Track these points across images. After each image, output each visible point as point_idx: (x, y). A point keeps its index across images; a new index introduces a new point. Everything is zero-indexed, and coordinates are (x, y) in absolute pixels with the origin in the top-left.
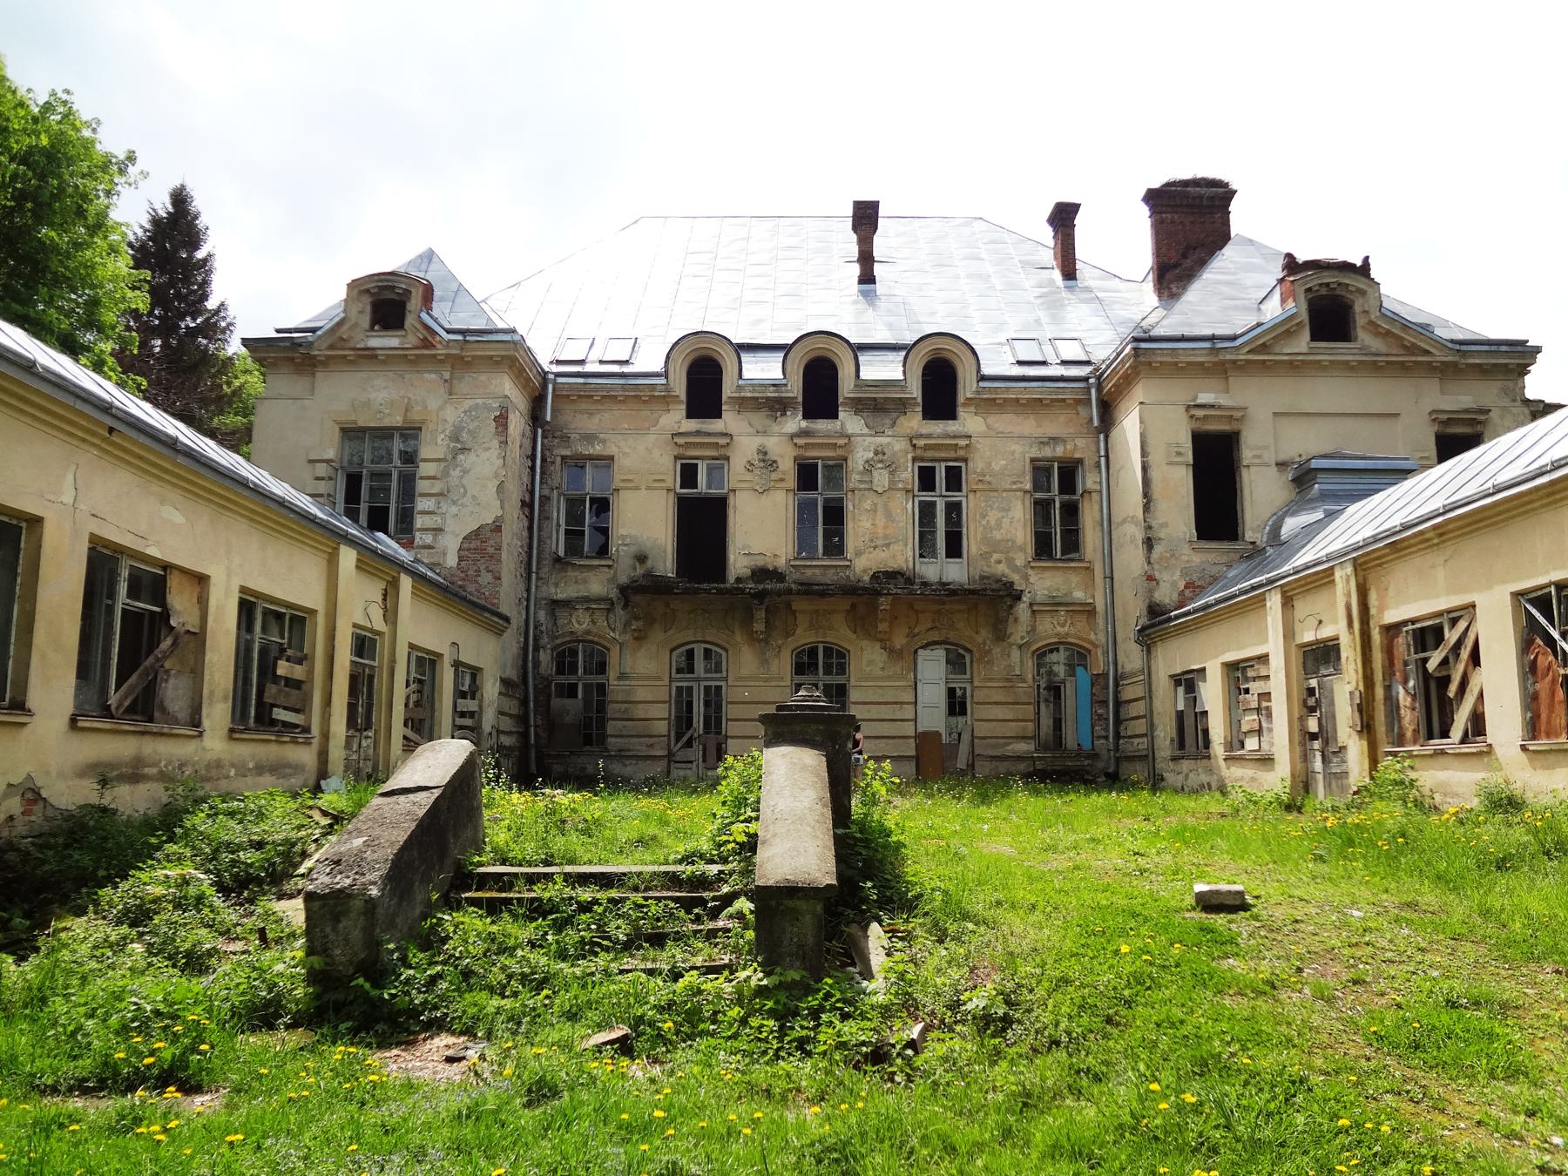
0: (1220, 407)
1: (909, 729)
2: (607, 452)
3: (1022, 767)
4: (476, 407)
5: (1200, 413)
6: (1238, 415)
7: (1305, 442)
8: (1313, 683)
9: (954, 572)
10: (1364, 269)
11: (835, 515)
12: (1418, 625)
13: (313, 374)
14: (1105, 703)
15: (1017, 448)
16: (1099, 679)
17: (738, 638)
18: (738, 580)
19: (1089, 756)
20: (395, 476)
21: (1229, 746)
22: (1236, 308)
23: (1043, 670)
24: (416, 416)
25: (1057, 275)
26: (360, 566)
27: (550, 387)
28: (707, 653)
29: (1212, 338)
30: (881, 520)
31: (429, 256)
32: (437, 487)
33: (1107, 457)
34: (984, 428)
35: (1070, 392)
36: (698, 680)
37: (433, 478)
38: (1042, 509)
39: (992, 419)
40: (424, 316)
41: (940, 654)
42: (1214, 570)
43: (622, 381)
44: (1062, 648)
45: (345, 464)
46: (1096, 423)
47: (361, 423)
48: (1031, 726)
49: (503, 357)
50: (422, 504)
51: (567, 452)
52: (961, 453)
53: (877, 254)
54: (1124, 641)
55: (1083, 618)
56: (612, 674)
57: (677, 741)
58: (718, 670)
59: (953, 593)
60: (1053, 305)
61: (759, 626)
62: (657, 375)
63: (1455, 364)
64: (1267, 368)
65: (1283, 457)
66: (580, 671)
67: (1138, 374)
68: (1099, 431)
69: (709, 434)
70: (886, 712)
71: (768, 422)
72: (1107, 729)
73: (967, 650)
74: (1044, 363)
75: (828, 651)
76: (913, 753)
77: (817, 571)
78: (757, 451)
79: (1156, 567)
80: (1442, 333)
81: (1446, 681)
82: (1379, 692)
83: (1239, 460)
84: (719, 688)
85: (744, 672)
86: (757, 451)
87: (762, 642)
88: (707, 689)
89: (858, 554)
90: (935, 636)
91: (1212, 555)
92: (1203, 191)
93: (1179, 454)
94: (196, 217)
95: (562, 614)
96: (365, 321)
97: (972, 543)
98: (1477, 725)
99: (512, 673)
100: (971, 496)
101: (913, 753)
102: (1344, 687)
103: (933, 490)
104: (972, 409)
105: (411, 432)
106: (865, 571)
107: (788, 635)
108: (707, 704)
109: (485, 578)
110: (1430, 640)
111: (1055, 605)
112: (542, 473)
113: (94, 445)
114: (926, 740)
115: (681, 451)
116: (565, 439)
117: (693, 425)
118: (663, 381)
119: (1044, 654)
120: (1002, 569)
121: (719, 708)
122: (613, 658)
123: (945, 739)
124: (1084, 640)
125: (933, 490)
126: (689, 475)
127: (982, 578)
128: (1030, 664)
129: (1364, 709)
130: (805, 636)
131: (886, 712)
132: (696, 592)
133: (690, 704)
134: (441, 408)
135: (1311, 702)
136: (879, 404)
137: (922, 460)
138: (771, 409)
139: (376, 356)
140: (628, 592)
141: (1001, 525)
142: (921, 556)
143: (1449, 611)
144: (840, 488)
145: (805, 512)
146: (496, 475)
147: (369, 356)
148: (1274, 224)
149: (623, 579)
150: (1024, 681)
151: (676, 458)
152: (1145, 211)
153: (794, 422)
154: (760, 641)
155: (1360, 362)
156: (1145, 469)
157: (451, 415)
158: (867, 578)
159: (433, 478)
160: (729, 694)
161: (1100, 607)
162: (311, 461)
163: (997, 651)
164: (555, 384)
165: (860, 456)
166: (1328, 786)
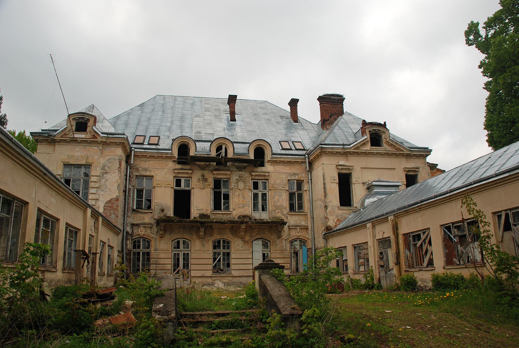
0: (346, 166)
1: (250, 267)
5: (340, 167)
7: (370, 177)
9: (264, 216)
10: (384, 125)
15: (284, 176)
17: (195, 237)
20: (82, 181)
23: (292, 247)
24: (90, 161)
28: (184, 242)
32: (97, 185)
33: (311, 180)
35: (300, 159)
36: (181, 251)
37: (96, 182)
38: (291, 195)
40: (94, 128)
41: (260, 242)
42: (345, 216)
43: (157, 151)
47: (71, 163)
49: (120, 143)
50: (92, 191)
51: (138, 174)
52: (266, 178)
53: (236, 111)
54: (318, 238)
55: (304, 230)
56: (152, 249)
57: (174, 271)
58: (188, 247)
59: (264, 223)
61: (202, 233)
63: (410, 154)
65: (364, 181)
66: (141, 247)
73: (268, 241)
74: (291, 149)
75: (224, 241)
77: (221, 215)
80: (406, 145)
83: (351, 182)
84: (188, 254)
85: (196, 248)
89: (234, 210)
91: (345, 211)
93: (334, 180)
95: (134, 228)
97: (270, 206)
98: (431, 263)
99: (120, 249)
103: (258, 189)
105: (88, 166)
106: (236, 215)
107: (211, 236)
108: (184, 259)
109: (113, 216)
110: (416, 238)
111: (295, 227)
112: (129, 181)
113: (39, 179)
115: (176, 175)
116: (137, 169)
118: (170, 152)
119: (292, 242)
120: (279, 215)
121: (188, 260)
122: (152, 243)
125: (258, 189)
126: (178, 183)
127: (273, 218)
128: (288, 245)
130: (217, 237)
132: (182, 222)
133: (178, 259)
134: (99, 158)
135: (382, 256)
137: (254, 179)
140: (158, 222)
141: (279, 202)
143: (422, 230)
144: (228, 188)
146: (117, 182)
147: (75, 141)
149: (156, 217)
150: (287, 251)
151: (174, 177)
152: (318, 103)
154: (202, 238)
157: (102, 161)
158: (237, 218)
159: (96, 182)
161: (310, 227)
163: (278, 241)
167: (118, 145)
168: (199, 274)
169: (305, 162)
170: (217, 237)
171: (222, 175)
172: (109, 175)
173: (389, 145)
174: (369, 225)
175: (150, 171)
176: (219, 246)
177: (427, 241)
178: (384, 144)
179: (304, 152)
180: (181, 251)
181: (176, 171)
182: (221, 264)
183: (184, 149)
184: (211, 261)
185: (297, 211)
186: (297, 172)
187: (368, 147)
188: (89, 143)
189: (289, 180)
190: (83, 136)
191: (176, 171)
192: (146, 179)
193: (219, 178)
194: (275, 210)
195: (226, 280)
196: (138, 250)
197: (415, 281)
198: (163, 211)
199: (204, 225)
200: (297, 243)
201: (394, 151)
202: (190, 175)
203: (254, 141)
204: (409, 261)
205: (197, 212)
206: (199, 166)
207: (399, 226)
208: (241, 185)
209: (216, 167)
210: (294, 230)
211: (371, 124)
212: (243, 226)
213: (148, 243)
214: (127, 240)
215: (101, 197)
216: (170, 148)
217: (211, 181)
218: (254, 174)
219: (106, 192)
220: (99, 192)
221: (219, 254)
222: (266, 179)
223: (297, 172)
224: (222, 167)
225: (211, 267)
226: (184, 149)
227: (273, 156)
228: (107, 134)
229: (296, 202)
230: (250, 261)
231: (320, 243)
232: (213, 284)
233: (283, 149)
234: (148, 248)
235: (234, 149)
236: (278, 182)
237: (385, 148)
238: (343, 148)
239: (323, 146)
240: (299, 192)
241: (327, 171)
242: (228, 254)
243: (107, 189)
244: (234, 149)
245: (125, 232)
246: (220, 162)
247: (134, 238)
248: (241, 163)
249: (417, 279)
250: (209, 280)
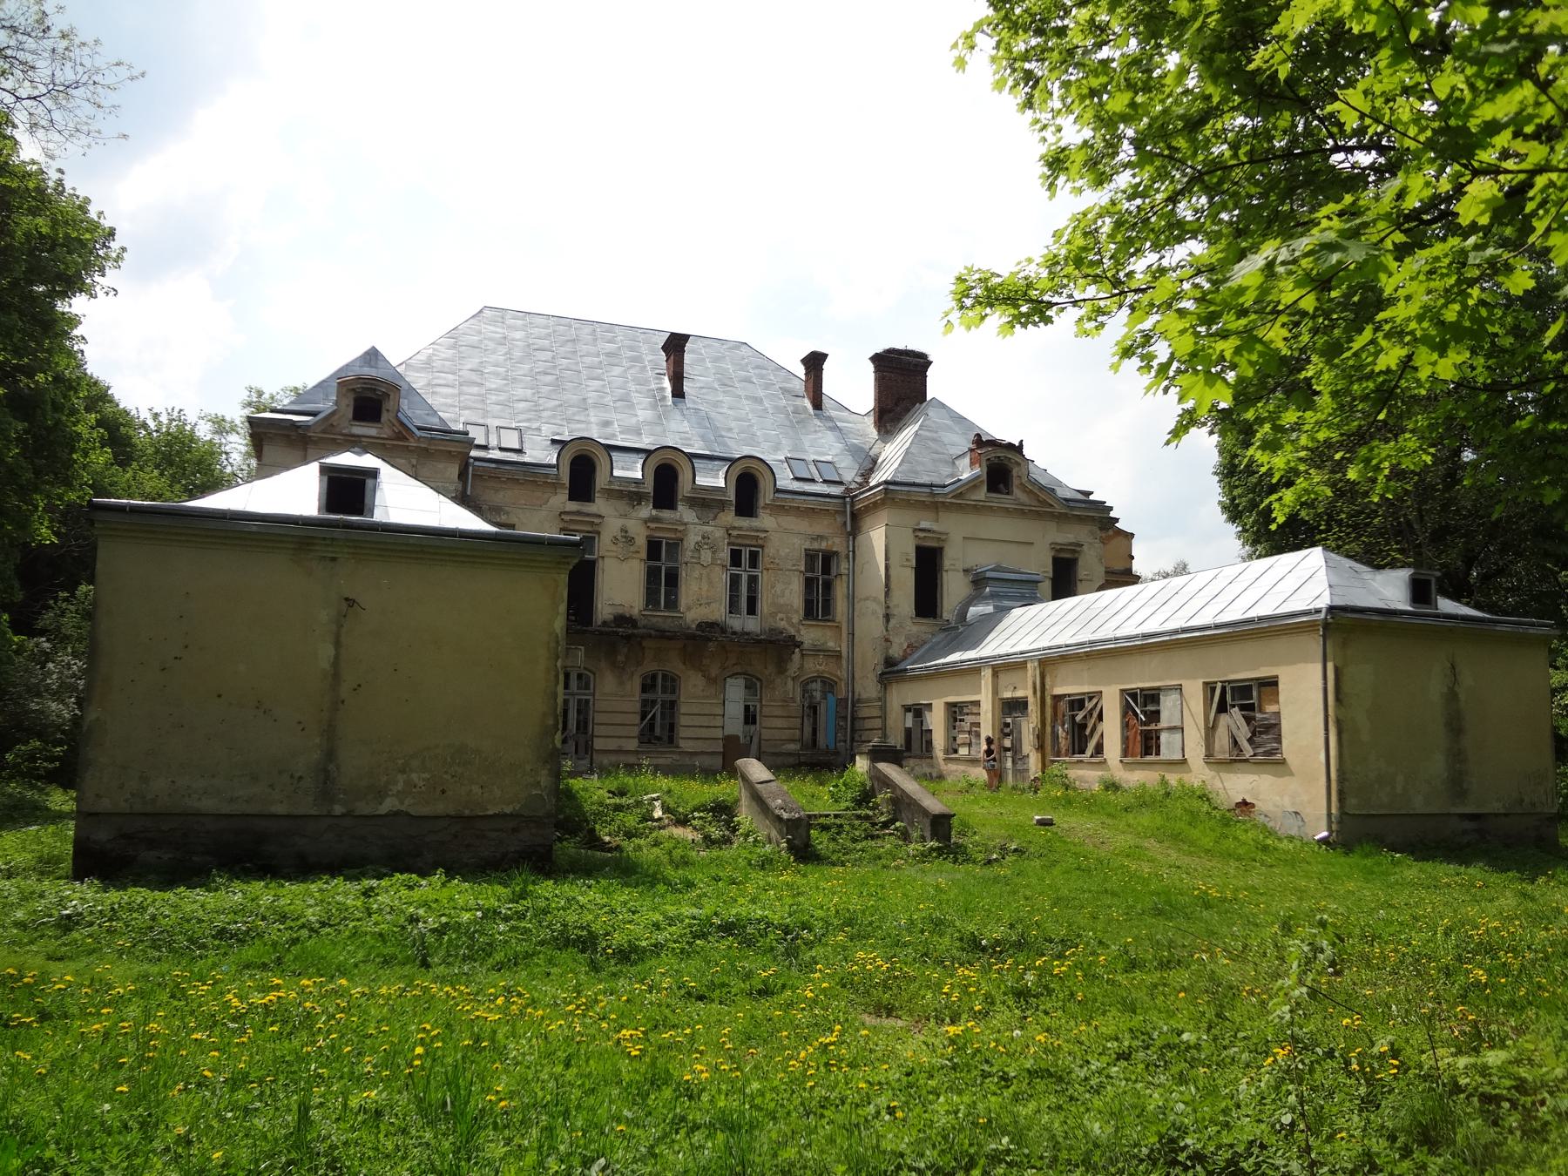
3: (791, 760)
5: (921, 534)
6: (942, 537)
7: (984, 558)
8: (1009, 720)
9: (751, 624)
10: (1019, 449)
11: (673, 579)
13: (305, 450)
15: (796, 541)
16: (842, 702)
18: (605, 623)
21: (946, 752)
22: (940, 461)
25: (807, 403)
28: (580, 676)
29: (932, 485)
30: (705, 587)
31: (373, 355)
38: (809, 583)
39: (780, 519)
41: (741, 682)
42: (925, 637)
48: (798, 732)
58: (587, 687)
60: (796, 422)
61: (620, 658)
62: (549, 466)
64: (960, 508)
65: (967, 566)
68: (849, 534)
69: (588, 515)
70: (704, 721)
71: (628, 508)
74: (813, 481)
75: (664, 676)
78: (619, 530)
81: (1085, 726)
82: (1048, 729)
84: (587, 701)
86: (619, 530)
88: (579, 701)
89: (689, 609)
90: (738, 669)
91: (921, 628)
96: (350, 413)
97: (764, 605)
98: (1099, 749)
102: (1028, 726)
108: (579, 712)
111: (817, 651)
117: (573, 506)
120: (783, 624)
129: (1040, 737)
130: (650, 666)
131: (704, 721)
136: (706, 502)
138: (631, 499)
141: (783, 593)
145: (652, 575)
152: (871, 367)
153: (646, 511)
156: (887, 568)
161: (844, 654)
163: (778, 681)
165: (692, 539)
166: (1015, 775)
168: (612, 744)
175: (508, 513)
176: (653, 686)
177: (1095, 715)
178: (1016, 490)
181: (567, 518)
184: (637, 719)
187: (982, 494)
210: (811, 659)
211: (994, 443)
221: (654, 702)
225: (635, 731)
231: (868, 687)
233: (797, 479)
242: (673, 704)
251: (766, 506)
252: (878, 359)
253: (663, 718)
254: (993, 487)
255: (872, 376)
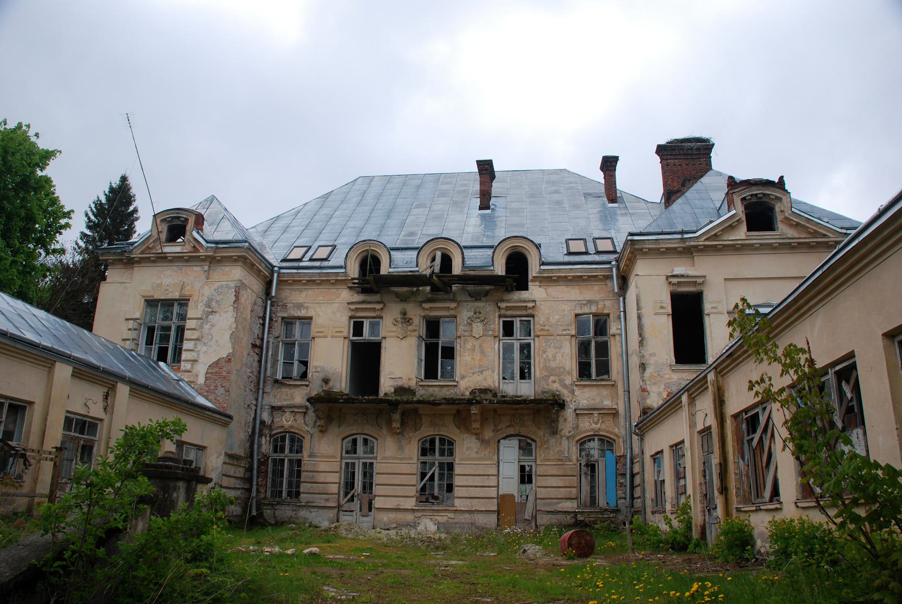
0: (688, 276)
1: (493, 493)
2: (309, 315)
4: (222, 286)
5: (674, 280)
9: (525, 389)
10: (780, 184)
12: (749, 414)
14: (624, 475)
15: (566, 307)
16: (619, 459)
17: (384, 431)
19: (613, 511)
20: (173, 329)
23: (583, 453)
26: (76, 374)
27: (275, 275)
28: (366, 441)
30: (477, 356)
32: (196, 335)
33: (625, 312)
34: (545, 295)
36: (359, 458)
38: (584, 348)
41: (515, 442)
43: (319, 271)
44: (596, 438)
45: (147, 321)
46: (616, 290)
47: (156, 297)
48: (574, 491)
49: (239, 257)
50: (186, 345)
51: (285, 315)
52: (530, 312)
55: (611, 418)
56: (305, 453)
62: (341, 267)
66: (287, 451)
67: (635, 257)
70: (478, 481)
72: (625, 493)
74: (586, 253)
75: (442, 441)
76: (495, 508)
77: (436, 389)
79: (648, 382)
85: (388, 454)
87: (398, 434)
88: (365, 464)
89: (463, 377)
90: (511, 431)
91: (687, 374)
92: (692, 145)
93: (662, 307)
94: (129, 190)
95: (277, 414)
97: (537, 370)
100: (537, 339)
101: (495, 508)
103: (512, 335)
104: (537, 283)
106: (466, 389)
107: (416, 429)
111: (589, 411)
112: (270, 327)
114: (504, 500)
115: (353, 313)
116: (285, 306)
118: (343, 270)
119: (582, 444)
120: (556, 387)
121: (371, 476)
122: (306, 444)
123: (517, 499)
124: (611, 433)
125: (512, 335)
126: (358, 328)
127: (543, 392)
128: (575, 450)
130: (427, 431)
131: (478, 481)
133: (353, 474)
134: (202, 287)
137: (505, 317)
139: (166, 257)
142: (504, 378)
146: (230, 327)
147: (163, 258)
148: (729, 162)
151: (351, 318)
152: (658, 159)
154: (398, 434)
155: (780, 244)
156: (639, 318)
157: (207, 291)
158: (467, 393)
160: (377, 468)
161: (621, 411)
162: (127, 319)
163: (552, 441)
164: (279, 273)
167: (236, 261)
168: (390, 503)
169: (611, 277)
170: (427, 431)
171: (437, 310)
172: (217, 315)
173: (791, 226)
174: (685, 398)
175: (307, 308)
176: (433, 450)
179: (612, 257)
180: (359, 458)
181: (353, 307)
182: (435, 487)
183: (370, 263)
184: (414, 479)
185: (594, 377)
186: (597, 297)
187: (741, 233)
188: (187, 261)
189: (577, 315)
190: (178, 249)
191: (353, 307)
192: (300, 323)
193: (436, 317)
194: (548, 377)
195: (442, 518)
196: (281, 456)
197: (751, 536)
198: (326, 381)
199: (404, 410)
200: (594, 447)
201: (804, 238)
202: (378, 313)
203: (504, 240)
204: (742, 483)
205: (391, 383)
206: (397, 295)
207: (727, 395)
208: (478, 329)
209: (430, 296)
211: (748, 183)
212: (474, 410)
213: (297, 442)
214: (261, 435)
215: (201, 355)
216: (343, 264)
217: (419, 326)
218: (503, 305)
219: (210, 346)
220: (199, 347)
221: (433, 464)
222: (529, 315)
223: (596, 298)
224: (441, 295)
225: (412, 491)
226: (370, 263)
227: (542, 267)
228: (217, 243)
229: (593, 359)
230: (493, 481)
232: (414, 525)
233: (570, 254)
234: (297, 452)
235: (463, 258)
236: (553, 320)
237: (783, 231)
238: (682, 239)
239: (636, 238)
240: (601, 339)
241: (651, 288)
242: (451, 466)
243: (215, 338)
244: (463, 258)
245: (258, 422)
246: (442, 283)
247: (274, 432)
248: (481, 285)
249: (755, 533)
250: (409, 517)
251: (535, 279)
252: (662, 150)
253: (441, 476)
254: (752, 226)
255: (659, 166)
